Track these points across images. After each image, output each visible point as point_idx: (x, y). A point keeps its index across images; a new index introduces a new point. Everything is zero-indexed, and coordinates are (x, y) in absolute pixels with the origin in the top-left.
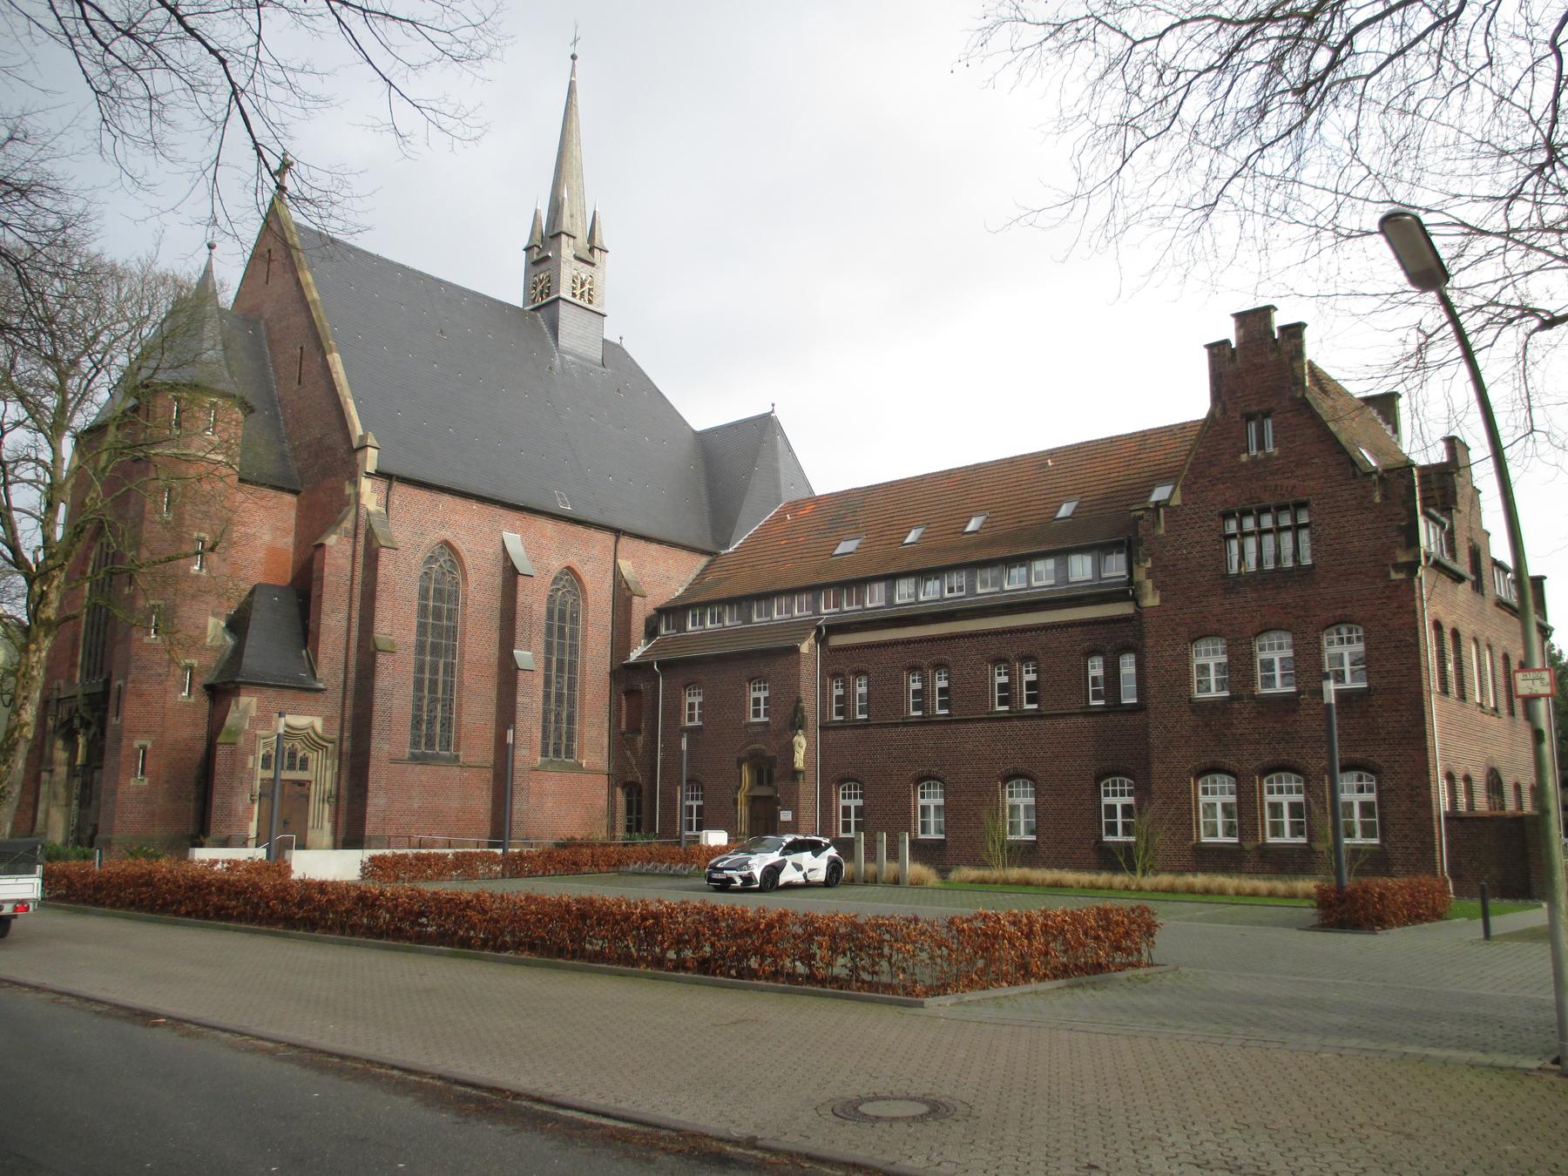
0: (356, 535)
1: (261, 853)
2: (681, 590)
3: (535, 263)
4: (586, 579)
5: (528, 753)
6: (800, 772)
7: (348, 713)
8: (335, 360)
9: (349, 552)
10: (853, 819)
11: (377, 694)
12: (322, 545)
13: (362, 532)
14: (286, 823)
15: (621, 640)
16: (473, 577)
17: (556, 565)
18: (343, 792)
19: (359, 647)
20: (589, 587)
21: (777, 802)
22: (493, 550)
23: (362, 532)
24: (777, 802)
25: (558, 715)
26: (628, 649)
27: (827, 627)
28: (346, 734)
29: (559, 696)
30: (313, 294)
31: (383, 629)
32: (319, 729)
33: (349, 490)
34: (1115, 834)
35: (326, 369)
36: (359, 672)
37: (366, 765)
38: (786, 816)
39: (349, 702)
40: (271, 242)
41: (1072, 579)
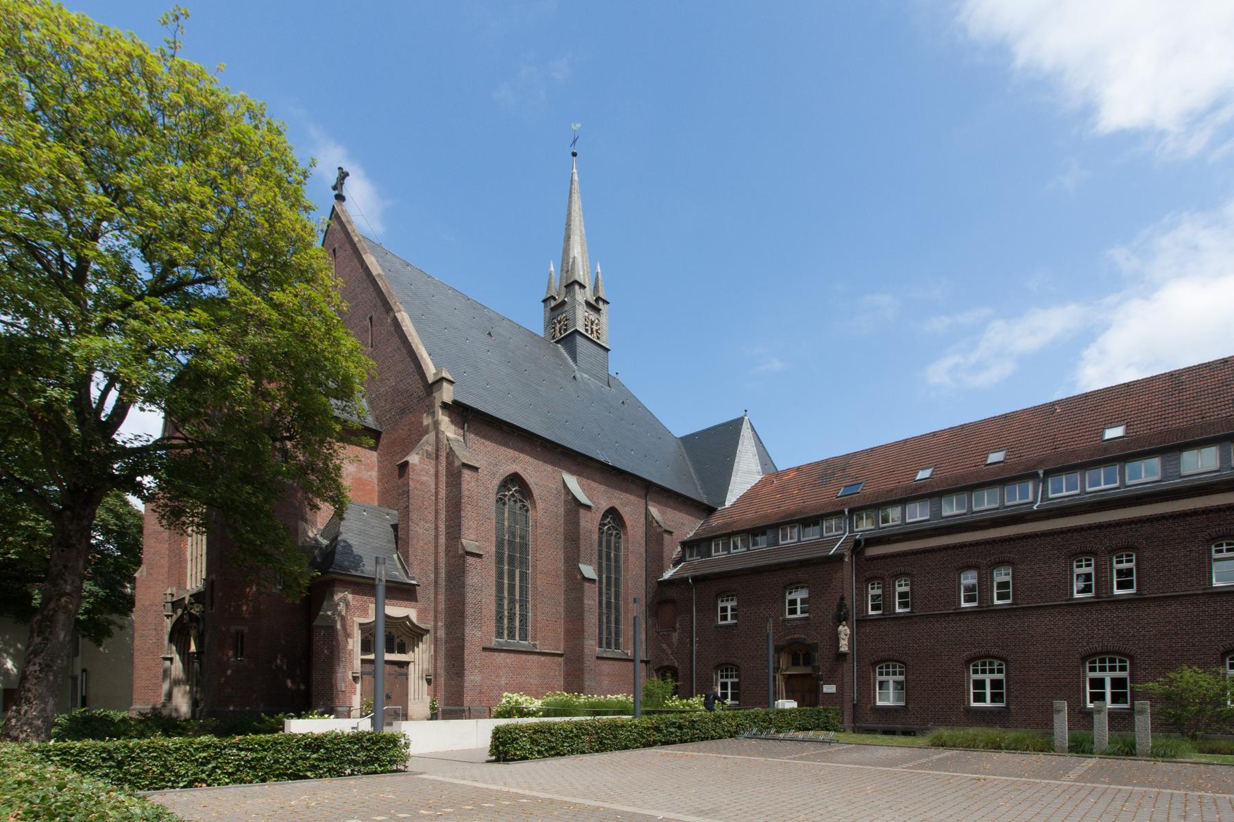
0: (437, 457)
1: (365, 725)
2: (691, 534)
3: (553, 309)
4: (626, 518)
5: (591, 645)
6: (844, 655)
7: (442, 606)
8: (404, 318)
9: (432, 471)
10: (729, 691)
11: (468, 590)
12: (407, 463)
13: (443, 455)
14: (388, 697)
15: (655, 560)
16: (540, 505)
17: (605, 505)
18: (441, 672)
19: (447, 551)
20: (628, 524)
21: (820, 678)
22: (554, 486)
23: (443, 455)
24: (820, 678)
25: (608, 618)
26: (662, 570)
27: (866, 540)
28: (440, 624)
29: (609, 604)
30: (376, 269)
31: (469, 542)
32: (414, 619)
33: (427, 421)
34: (984, 701)
35: (397, 325)
36: (448, 573)
37: (462, 648)
38: (829, 689)
39: (442, 598)
40: (334, 224)
41: (1184, 472)
